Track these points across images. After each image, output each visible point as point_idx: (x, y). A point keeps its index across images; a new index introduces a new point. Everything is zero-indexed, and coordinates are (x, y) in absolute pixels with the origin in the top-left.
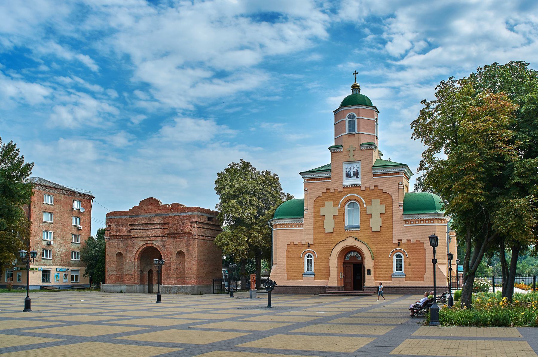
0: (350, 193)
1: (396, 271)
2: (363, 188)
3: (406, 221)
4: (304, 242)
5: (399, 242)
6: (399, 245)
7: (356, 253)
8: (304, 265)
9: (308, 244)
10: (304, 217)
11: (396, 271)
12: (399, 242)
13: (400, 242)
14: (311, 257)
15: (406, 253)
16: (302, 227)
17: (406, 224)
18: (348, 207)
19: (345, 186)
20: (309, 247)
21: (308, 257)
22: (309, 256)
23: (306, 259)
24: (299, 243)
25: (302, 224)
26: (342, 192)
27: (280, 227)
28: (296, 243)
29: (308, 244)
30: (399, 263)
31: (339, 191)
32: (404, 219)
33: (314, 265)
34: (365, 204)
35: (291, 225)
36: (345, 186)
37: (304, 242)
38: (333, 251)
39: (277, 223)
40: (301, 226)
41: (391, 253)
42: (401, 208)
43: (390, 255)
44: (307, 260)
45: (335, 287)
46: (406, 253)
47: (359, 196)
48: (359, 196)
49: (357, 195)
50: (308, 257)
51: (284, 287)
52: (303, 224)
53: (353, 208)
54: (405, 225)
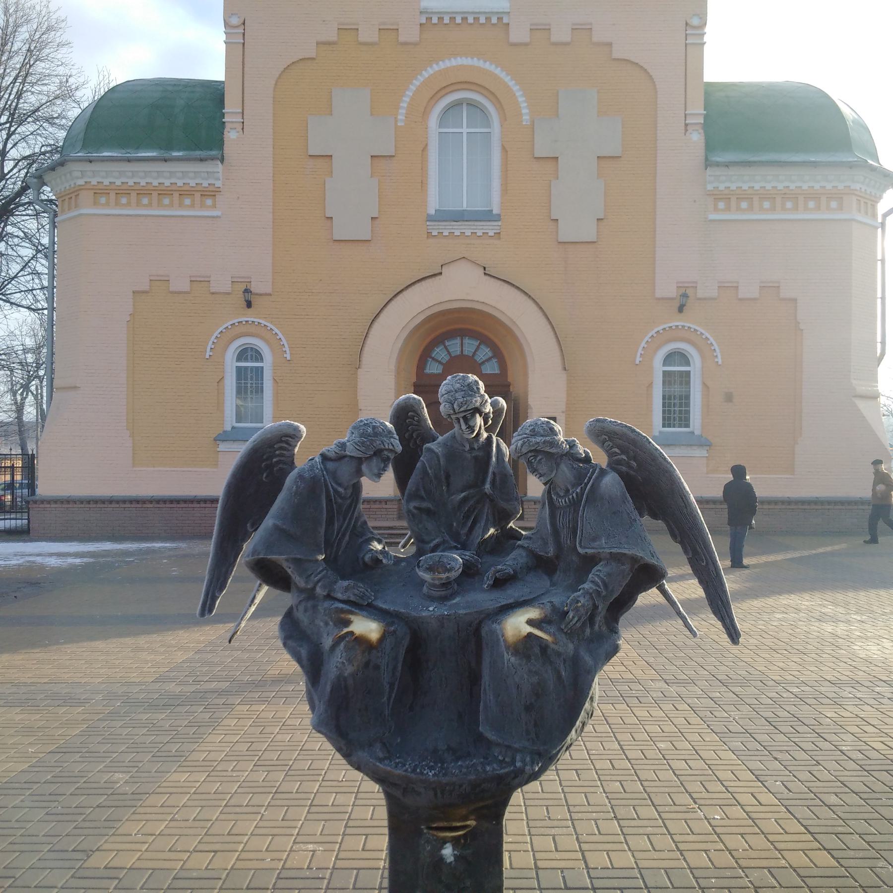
0: (455, 55)
1: (664, 426)
2: (519, 34)
3: (717, 197)
4: (221, 283)
5: (685, 296)
6: (681, 309)
7: (458, 341)
8: (220, 393)
9: (247, 291)
10: (222, 160)
11: (664, 426)
12: (685, 296)
13: (690, 292)
14: (258, 356)
15: (716, 346)
16: (214, 206)
17: (716, 209)
18: (443, 121)
19: (429, 19)
20: (249, 304)
21: (239, 359)
22: (244, 354)
23: (231, 364)
24: (451, 234)
25: (211, 193)
26: (415, 44)
27: (96, 203)
28: (180, 284)
29: (247, 291)
30: (677, 389)
31: (402, 39)
32: (710, 187)
33: (276, 395)
34: (525, 111)
35: (155, 194)
36: (429, 19)
37: (221, 283)
38: (376, 325)
39: (81, 182)
40: (209, 202)
41: (643, 344)
42: (697, 137)
43: (640, 351)
44: (239, 369)
45: (386, 501)
46: (716, 346)
47: (498, 71)
48: (498, 71)
49: (487, 66)
50: (239, 359)
51: (118, 502)
52: (218, 191)
53: (465, 130)
54: (712, 217)
